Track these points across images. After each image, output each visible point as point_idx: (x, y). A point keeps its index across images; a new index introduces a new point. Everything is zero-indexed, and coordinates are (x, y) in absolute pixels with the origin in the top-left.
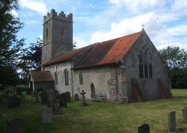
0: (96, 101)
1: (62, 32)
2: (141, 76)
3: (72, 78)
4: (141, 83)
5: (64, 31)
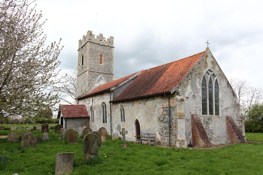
1: (101, 59)
2: (204, 112)
3: (111, 113)
4: (204, 121)
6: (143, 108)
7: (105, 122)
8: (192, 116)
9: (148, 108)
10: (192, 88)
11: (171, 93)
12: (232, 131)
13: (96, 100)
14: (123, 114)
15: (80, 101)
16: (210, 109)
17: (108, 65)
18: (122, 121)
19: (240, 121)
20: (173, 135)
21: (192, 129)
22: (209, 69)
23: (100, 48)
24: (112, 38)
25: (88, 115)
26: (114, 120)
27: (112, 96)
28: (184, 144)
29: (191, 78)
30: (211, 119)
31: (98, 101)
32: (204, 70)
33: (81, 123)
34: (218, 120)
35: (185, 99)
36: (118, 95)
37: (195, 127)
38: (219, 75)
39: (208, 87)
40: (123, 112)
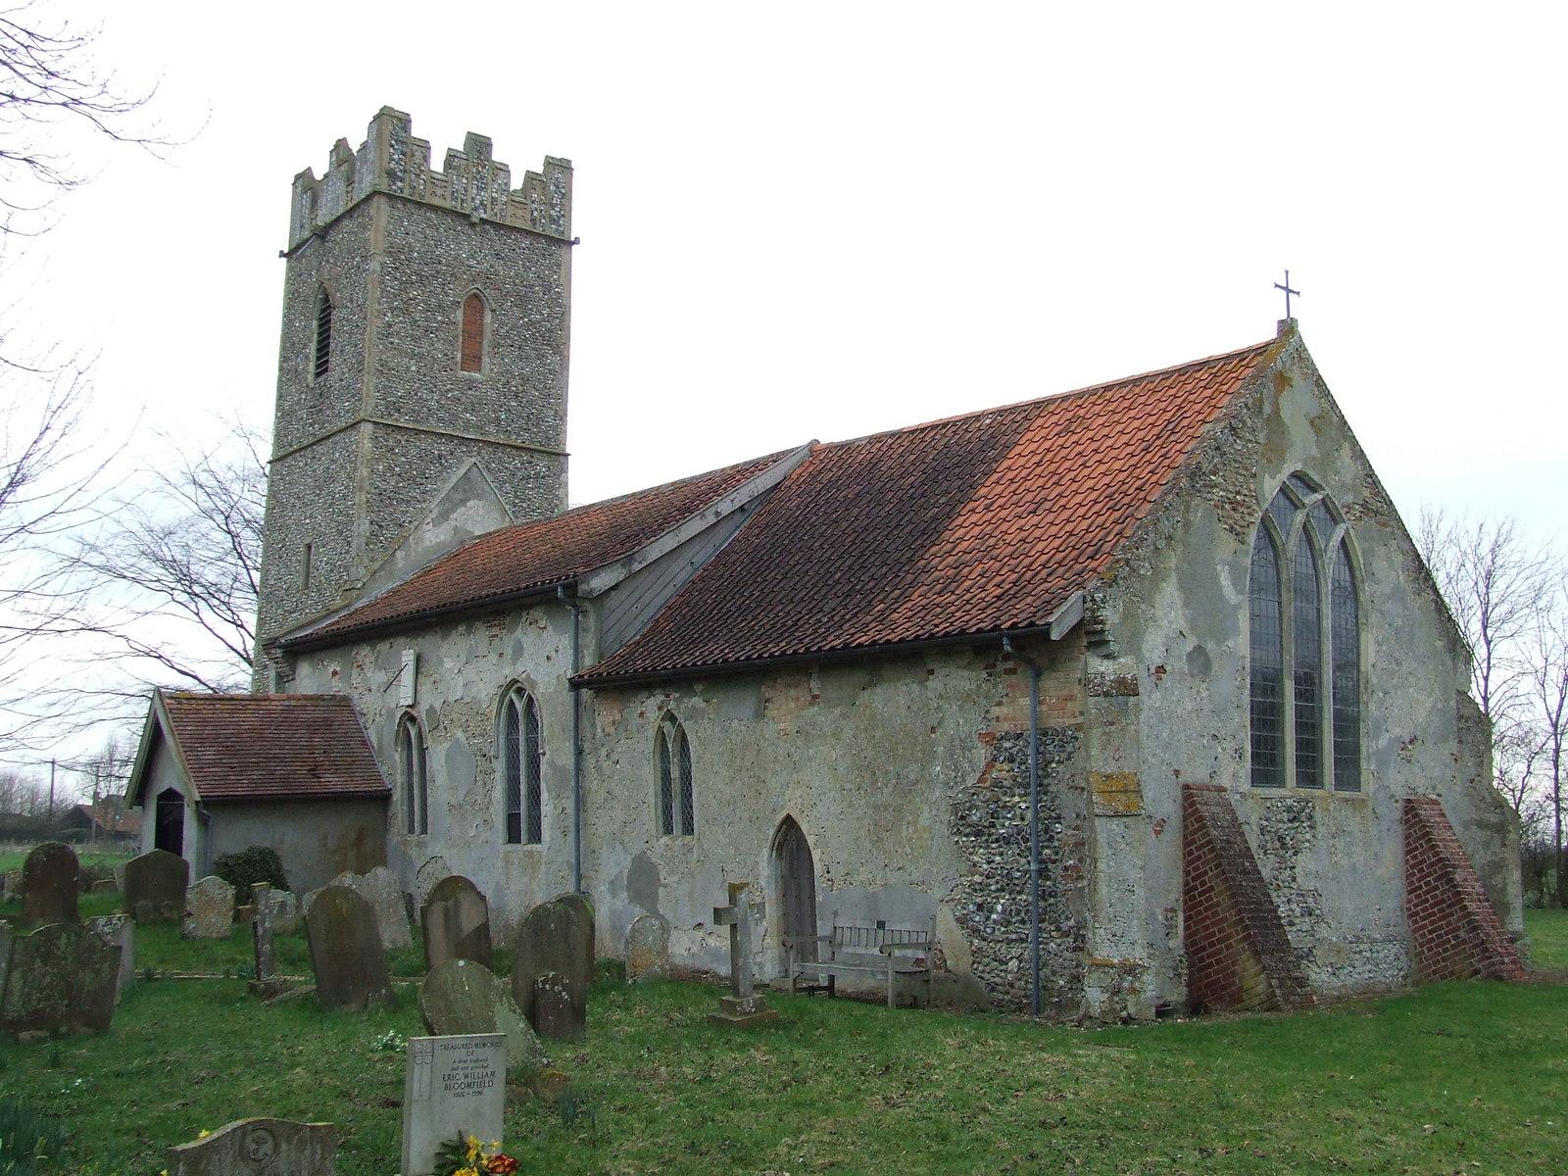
0: (830, 988)
1: (473, 333)
2: (1266, 769)
3: (579, 768)
4: (1263, 830)
5: (488, 317)
6: (837, 734)
8: (1191, 796)
9: (878, 734)
10: (1186, 604)
11: (1055, 636)
12: (1443, 901)
13: (448, 664)
14: (675, 773)
15: (304, 669)
16: (1301, 745)
17: (525, 380)
18: (668, 830)
20: (1058, 929)
21: (1188, 890)
22: (1299, 467)
23: (463, 248)
24: (559, 170)
25: (378, 778)
26: (602, 822)
27: (589, 640)
28: (1133, 991)
29: (1180, 532)
30: (1310, 818)
31: (470, 672)
33: (325, 837)
35: (1145, 685)
36: (633, 632)
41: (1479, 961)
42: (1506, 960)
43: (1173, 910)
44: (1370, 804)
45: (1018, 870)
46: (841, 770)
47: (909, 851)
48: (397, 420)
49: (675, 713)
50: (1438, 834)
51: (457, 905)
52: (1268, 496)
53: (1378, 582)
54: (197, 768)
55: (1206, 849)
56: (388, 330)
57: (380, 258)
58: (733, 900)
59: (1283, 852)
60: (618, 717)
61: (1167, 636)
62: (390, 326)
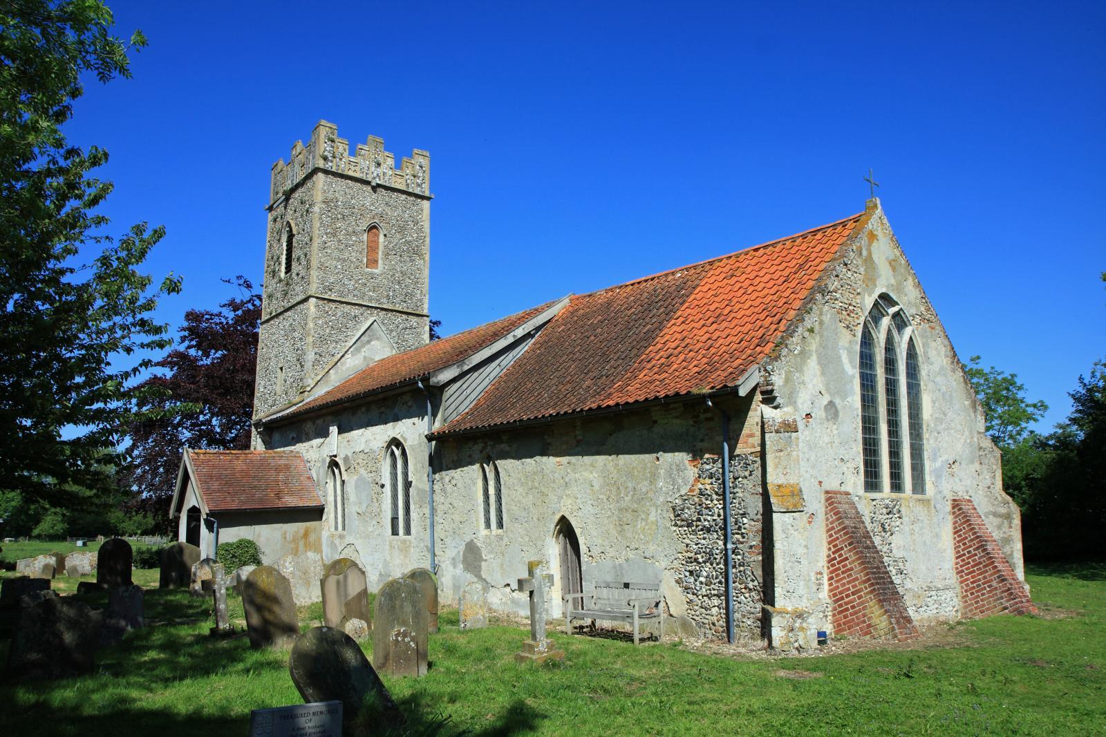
1: (372, 248)
2: (872, 482)
7: (401, 531)
10: (823, 374)
14: (492, 491)
19: (1001, 516)
22: (884, 290)
28: (802, 629)
32: (866, 296)
34: (920, 510)
37: (842, 549)
38: (918, 319)
39: (883, 370)
40: (492, 483)
41: (1008, 601)
42: (1024, 600)
43: (821, 573)
44: (932, 503)
45: (717, 549)
46: (597, 487)
47: (643, 537)
48: (330, 296)
49: (490, 454)
50: (974, 521)
51: (346, 577)
52: (867, 307)
53: (932, 364)
54: (207, 492)
55: (842, 533)
56: (324, 246)
57: (319, 205)
58: (531, 573)
59: (883, 534)
60: (455, 458)
61: (812, 394)
62: (326, 243)
